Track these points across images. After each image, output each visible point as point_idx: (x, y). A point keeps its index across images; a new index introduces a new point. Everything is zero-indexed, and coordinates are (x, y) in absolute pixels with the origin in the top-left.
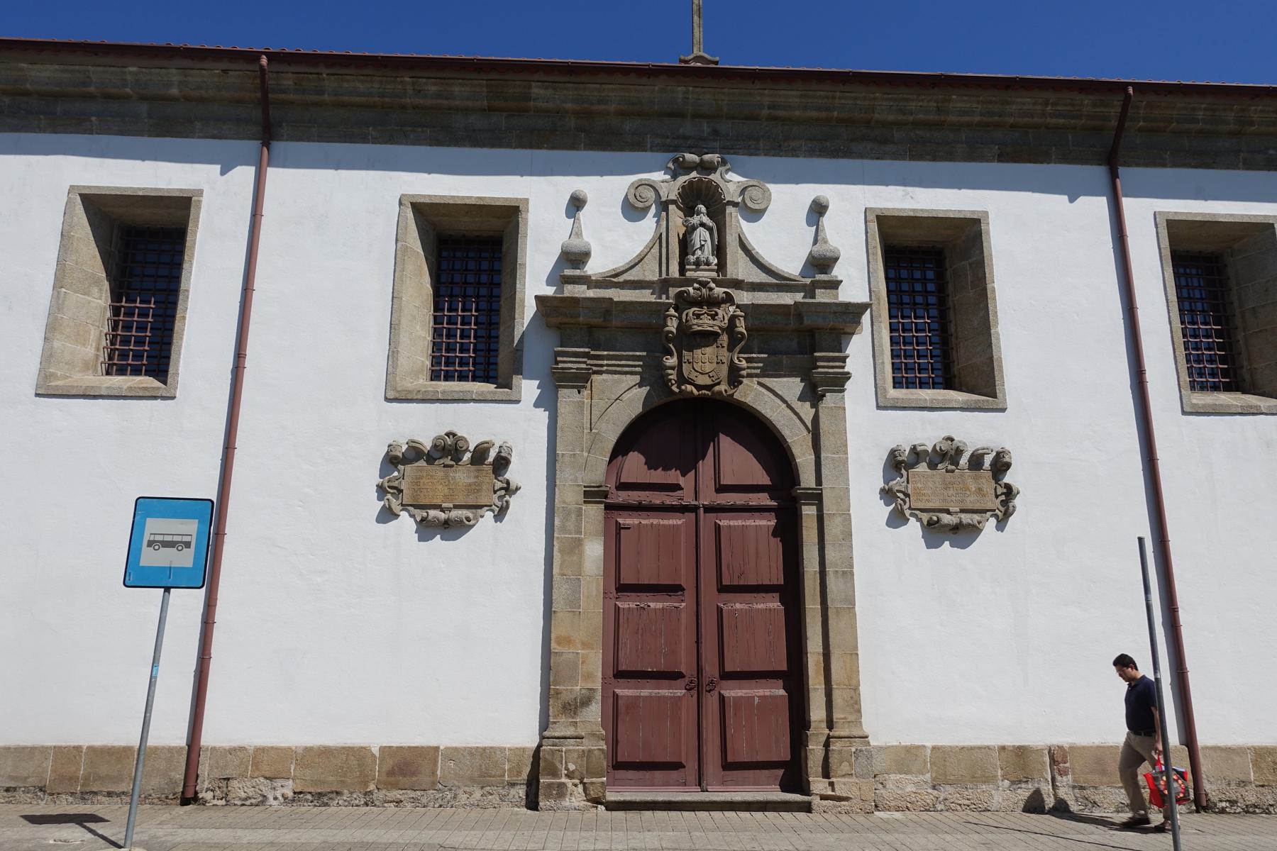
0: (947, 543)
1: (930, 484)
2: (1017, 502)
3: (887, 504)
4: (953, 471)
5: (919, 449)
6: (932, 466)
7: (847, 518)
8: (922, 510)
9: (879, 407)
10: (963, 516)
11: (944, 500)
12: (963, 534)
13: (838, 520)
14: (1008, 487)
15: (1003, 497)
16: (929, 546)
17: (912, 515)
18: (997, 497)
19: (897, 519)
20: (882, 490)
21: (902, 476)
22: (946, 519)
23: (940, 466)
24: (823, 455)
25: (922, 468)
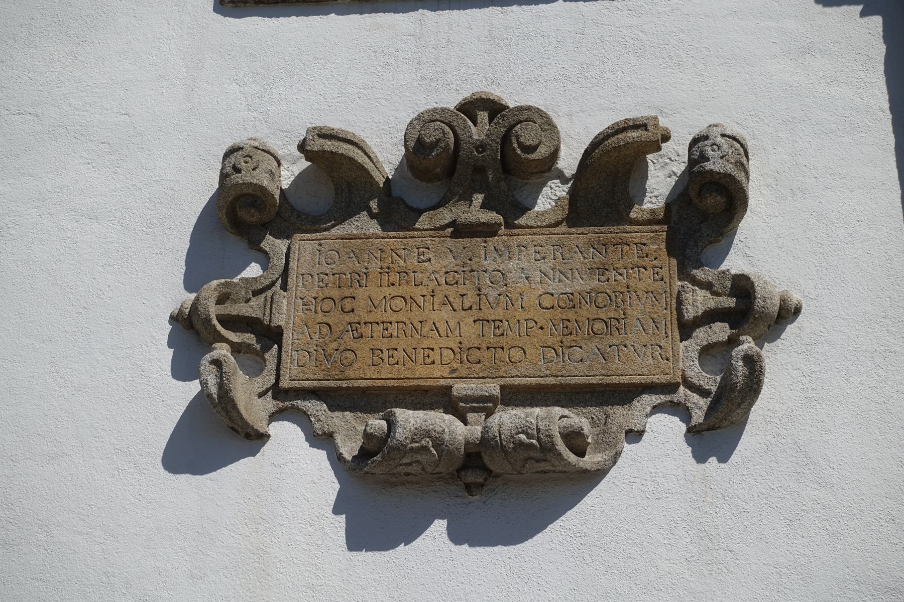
18: (686, 329)
19: (213, 436)
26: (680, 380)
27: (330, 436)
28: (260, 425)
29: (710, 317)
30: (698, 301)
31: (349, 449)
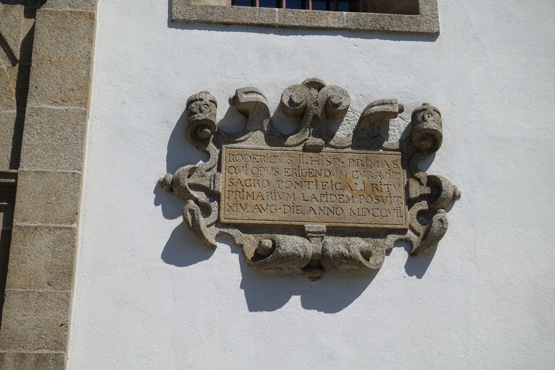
0: (296, 300)
1: (267, 175)
2: (454, 216)
3: (169, 215)
4: (317, 149)
5: (244, 98)
6: (275, 138)
7: (67, 239)
8: (246, 228)
9: (173, 22)
10: (329, 240)
11: (295, 208)
12: (325, 276)
13: (44, 241)
14: (435, 183)
15: (423, 205)
16: (255, 305)
17: (220, 237)
18: (410, 203)
19: (187, 247)
20: (162, 184)
21: (207, 156)
22: (291, 244)
23: (292, 140)
24: (31, 104)
25: (255, 140)
26: (408, 227)
27: (242, 246)
28: (213, 241)
29: (422, 197)
30: (416, 190)
31: (250, 254)
